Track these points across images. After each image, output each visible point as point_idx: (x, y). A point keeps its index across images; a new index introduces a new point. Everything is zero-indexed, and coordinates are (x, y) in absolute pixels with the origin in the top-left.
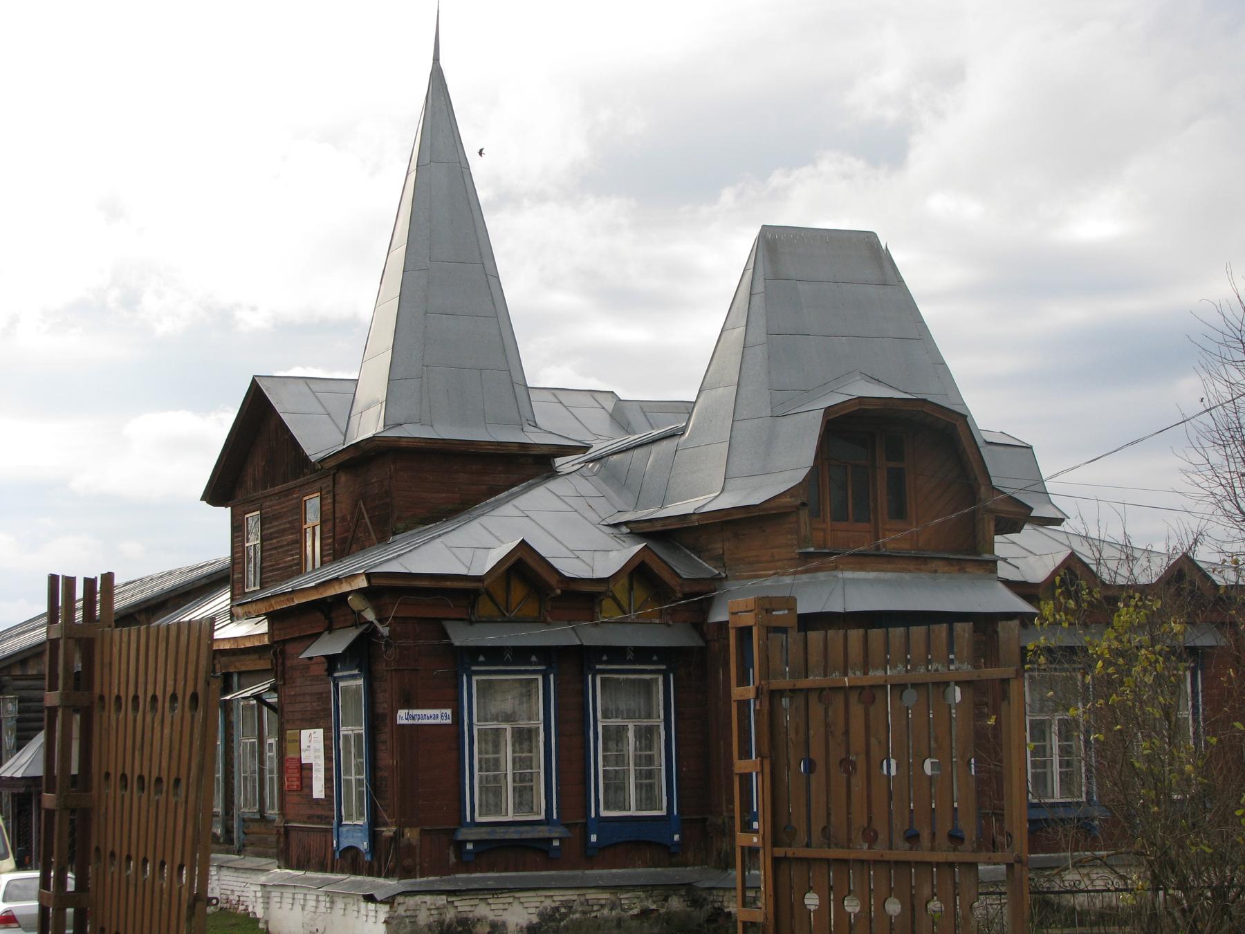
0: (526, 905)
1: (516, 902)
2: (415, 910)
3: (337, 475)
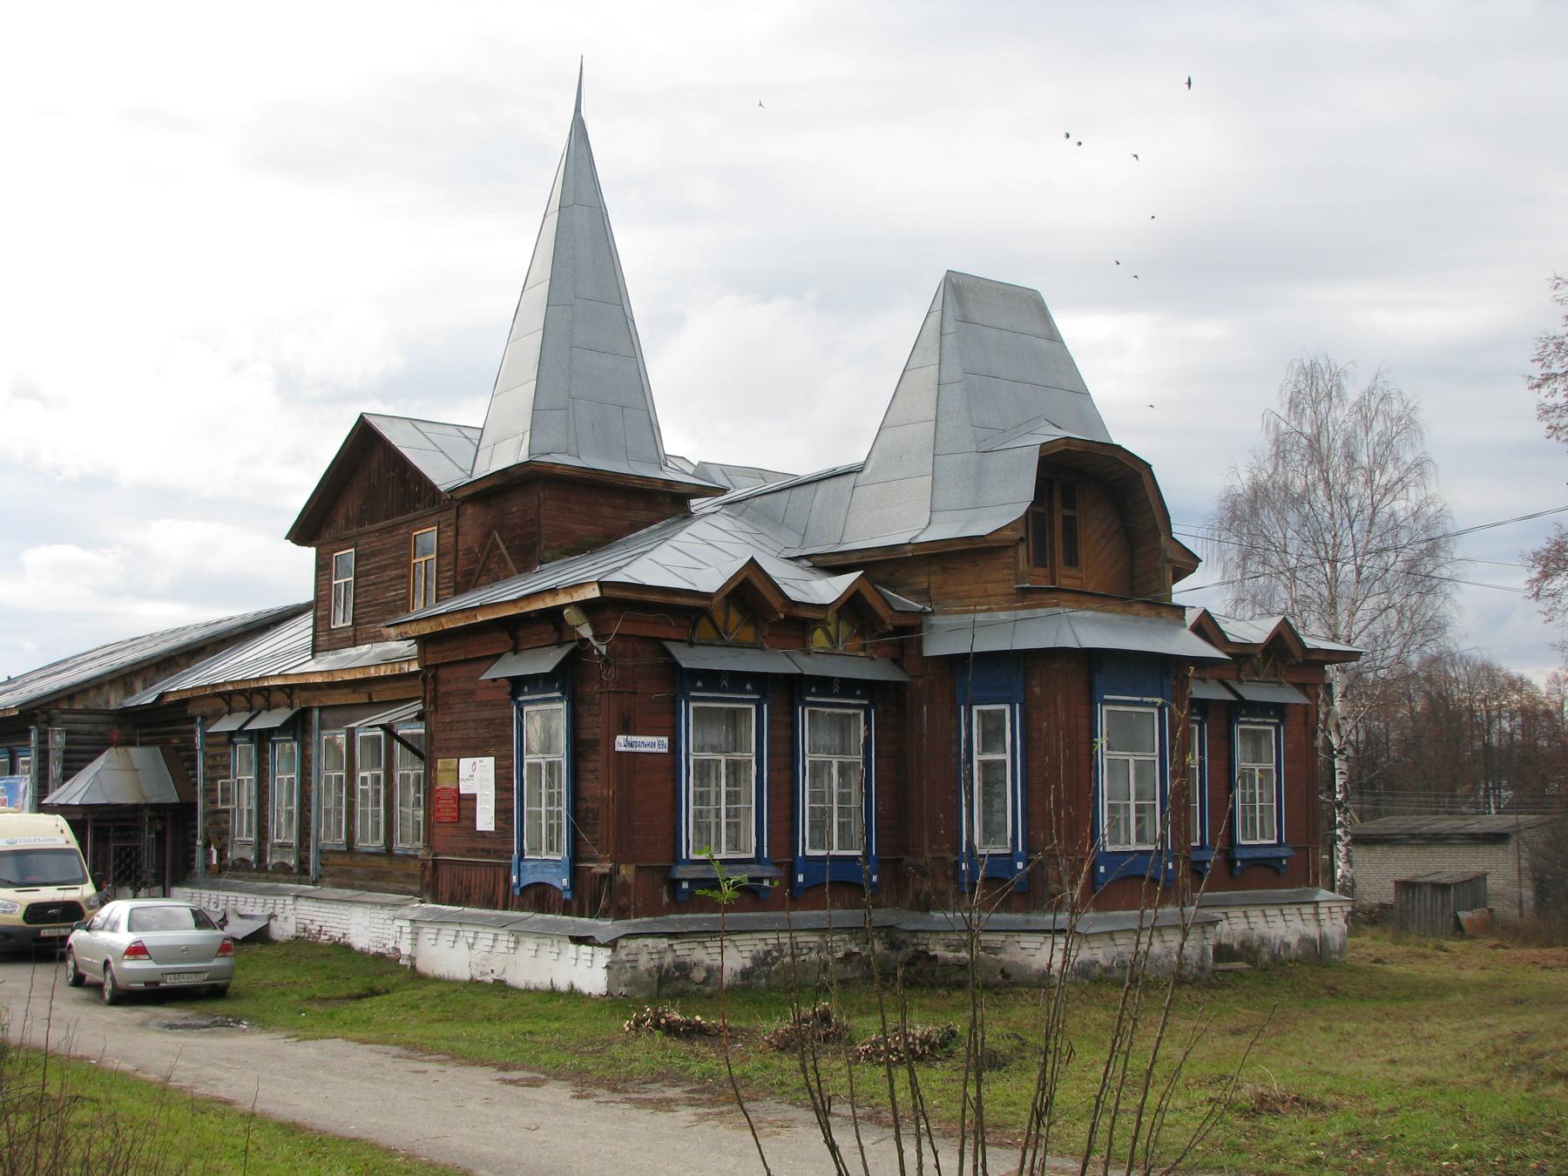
0: (740, 949)
1: (732, 944)
2: (636, 954)
3: (462, 508)
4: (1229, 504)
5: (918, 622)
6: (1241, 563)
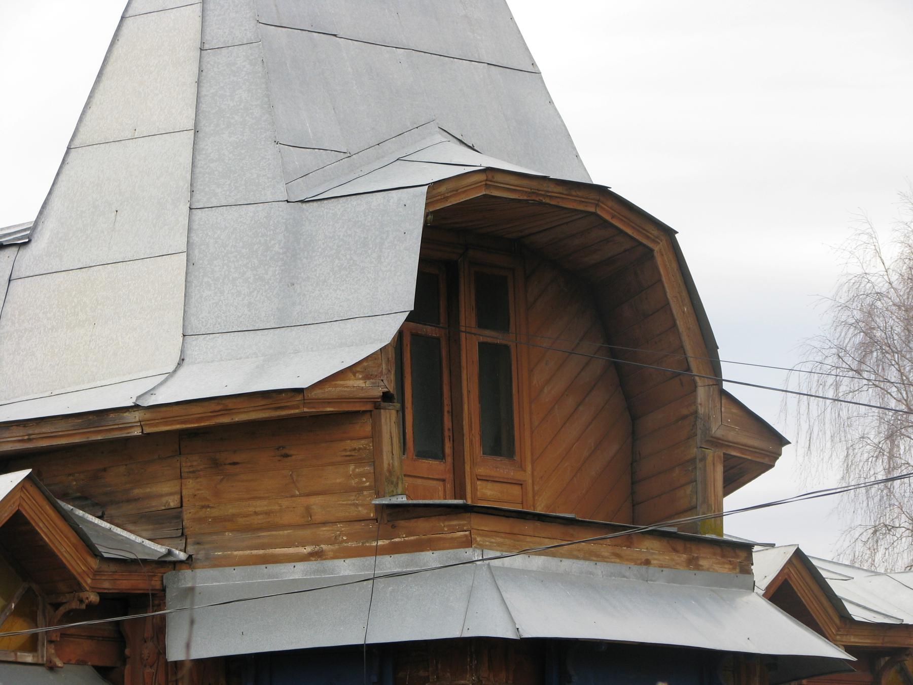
4: (858, 315)
5: (156, 584)
6: (886, 446)
